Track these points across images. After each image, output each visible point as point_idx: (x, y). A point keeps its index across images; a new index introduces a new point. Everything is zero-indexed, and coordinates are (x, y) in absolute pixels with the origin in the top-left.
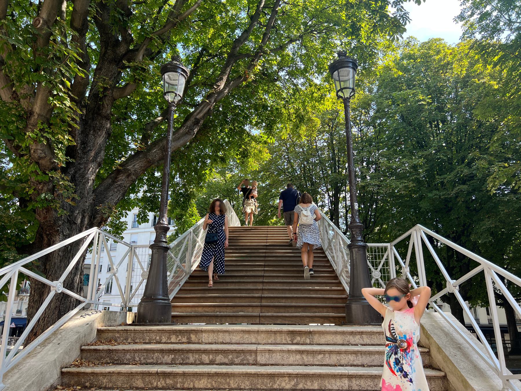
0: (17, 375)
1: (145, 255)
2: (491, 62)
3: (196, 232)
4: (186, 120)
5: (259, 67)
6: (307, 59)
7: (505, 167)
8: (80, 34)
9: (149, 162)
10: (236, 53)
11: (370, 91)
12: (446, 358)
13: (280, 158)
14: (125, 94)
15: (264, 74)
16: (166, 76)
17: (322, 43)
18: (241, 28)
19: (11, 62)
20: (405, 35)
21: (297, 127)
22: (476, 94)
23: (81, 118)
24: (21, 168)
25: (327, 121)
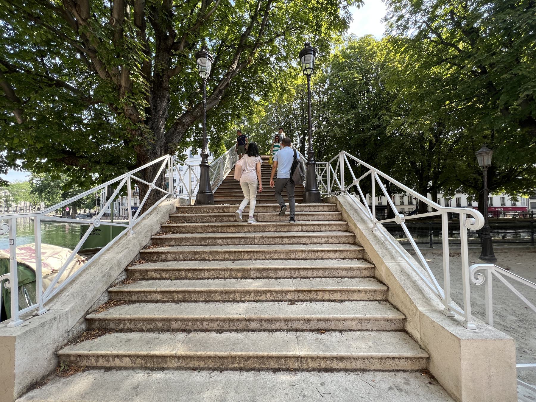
0: (139, 228)
1: (198, 171)
2: (399, 52)
3: (225, 158)
4: (214, 90)
5: (258, 55)
6: (288, 48)
7: (399, 120)
8: (141, 30)
9: (194, 117)
10: (243, 45)
11: (326, 71)
12: (349, 215)
13: (272, 115)
14: (176, 73)
15: (261, 59)
16: (199, 60)
17: (298, 37)
18: (246, 26)
19: (100, 51)
20: (350, 31)
21: (281, 95)
22: (388, 74)
23: (151, 90)
24: (121, 121)
25: (300, 91)
